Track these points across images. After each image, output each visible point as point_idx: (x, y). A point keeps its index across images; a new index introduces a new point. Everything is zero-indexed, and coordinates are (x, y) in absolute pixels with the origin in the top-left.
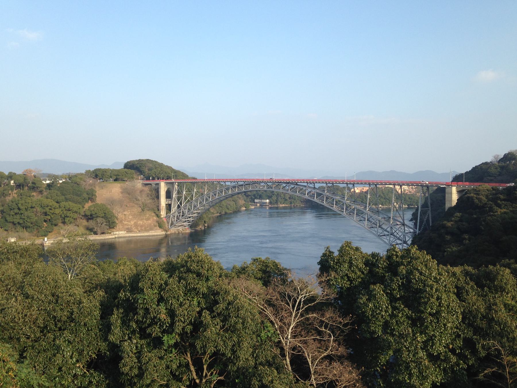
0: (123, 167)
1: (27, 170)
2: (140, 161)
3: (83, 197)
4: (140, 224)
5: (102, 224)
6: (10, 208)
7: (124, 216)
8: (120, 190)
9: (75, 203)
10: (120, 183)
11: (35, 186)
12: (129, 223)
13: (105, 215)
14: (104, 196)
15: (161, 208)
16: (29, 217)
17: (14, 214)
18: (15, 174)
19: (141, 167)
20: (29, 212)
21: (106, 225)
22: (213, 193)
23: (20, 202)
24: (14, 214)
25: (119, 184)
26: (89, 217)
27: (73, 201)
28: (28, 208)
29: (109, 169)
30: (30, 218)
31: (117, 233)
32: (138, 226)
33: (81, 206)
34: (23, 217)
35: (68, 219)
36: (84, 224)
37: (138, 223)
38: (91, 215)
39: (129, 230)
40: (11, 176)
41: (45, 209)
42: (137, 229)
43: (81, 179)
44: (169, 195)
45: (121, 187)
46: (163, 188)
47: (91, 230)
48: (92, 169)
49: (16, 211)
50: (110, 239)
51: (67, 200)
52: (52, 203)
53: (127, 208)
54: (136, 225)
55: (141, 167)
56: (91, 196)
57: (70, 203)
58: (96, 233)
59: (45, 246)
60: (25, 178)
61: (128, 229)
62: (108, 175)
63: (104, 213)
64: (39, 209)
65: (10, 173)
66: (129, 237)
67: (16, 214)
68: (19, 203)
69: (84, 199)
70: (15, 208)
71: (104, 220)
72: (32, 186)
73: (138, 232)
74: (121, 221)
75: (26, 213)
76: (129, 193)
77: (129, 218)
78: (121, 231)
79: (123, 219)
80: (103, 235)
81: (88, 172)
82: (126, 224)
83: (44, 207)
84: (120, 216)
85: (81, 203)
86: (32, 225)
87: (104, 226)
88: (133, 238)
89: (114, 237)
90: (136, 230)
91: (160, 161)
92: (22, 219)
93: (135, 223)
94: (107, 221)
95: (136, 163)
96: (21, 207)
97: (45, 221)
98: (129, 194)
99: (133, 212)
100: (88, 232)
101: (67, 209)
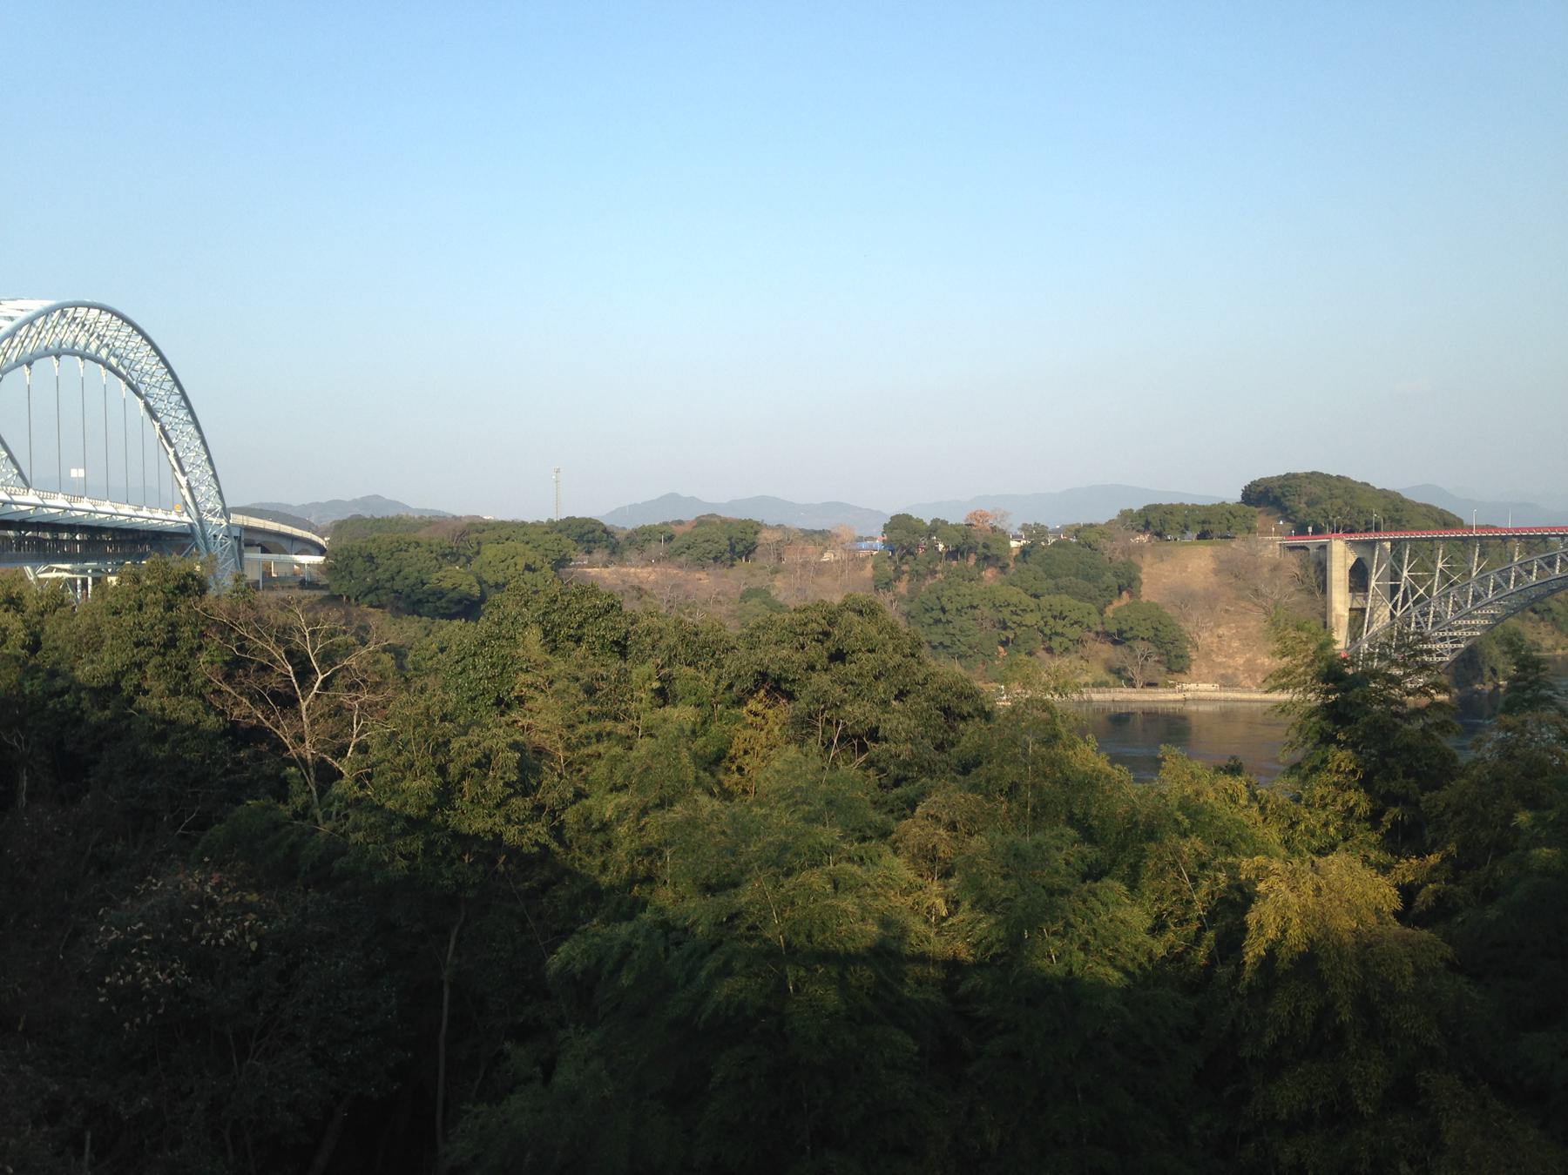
0: (1239, 499)
1: (975, 514)
2: (1286, 480)
3: (1103, 583)
4: (1263, 664)
5: (1146, 659)
6: (924, 607)
7: (1216, 640)
8: (1213, 566)
9: (1079, 601)
10: (1212, 545)
11: (989, 554)
12: (1231, 661)
13: (1156, 635)
14: (1164, 580)
15: (1334, 620)
16: (964, 631)
17: (931, 621)
18: (945, 523)
19: (1286, 496)
20: (965, 617)
21: (1158, 661)
22: (1498, 573)
23: (946, 593)
24: (931, 621)
25: (1209, 548)
26: (1118, 638)
27: (1074, 595)
28: (962, 608)
29: (1182, 504)
30: (967, 633)
31: (1193, 686)
32: (1257, 672)
33: (1093, 609)
34: (952, 631)
35: (1059, 639)
36: (1104, 655)
37: (1259, 661)
38: (1120, 632)
39: (1227, 682)
40: (938, 527)
41: (1001, 611)
42: (1253, 679)
43: (1102, 534)
44: (1359, 577)
45: (1215, 557)
46: (1341, 556)
47: (1120, 675)
48: (1137, 507)
49: (937, 614)
50: (1170, 701)
51: (1058, 589)
52: (1017, 596)
53: (1226, 615)
54: (1251, 668)
55: (1286, 496)
56: (1128, 582)
57: (1065, 597)
58: (1131, 683)
59: (249, 559)
60: (966, 533)
61: (1223, 676)
62: (1178, 523)
63: (1153, 628)
64: (987, 611)
65: (935, 521)
66: (1226, 700)
67: (938, 621)
68: (942, 596)
69: (1105, 590)
70: (935, 608)
71: (1153, 649)
72: (983, 553)
73: (1255, 688)
74: (1208, 654)
75: (958, 622)
76: (1236, 574)
77: (1230, 646)
78: (1205, 682)
79: (1215, 649)
80: (1148, 690)
81: (1126, 515)
82: (1220, 663)
83: (1001, 606)
84: (1205, 638)
85: (1095, 599)
86: (971, 652)
87: (1154, 669)
88: (1239, 704)
89: (1180, 696)
90: (1249, 682)
91: (1333, 471)
92: (950, 634)
93: (1248, 660)
94: (1161, 651)
95: (1276, 484)
96: (948, 606)
97: (1004, 644)
98: (1236, 576)
99: (1245, 628)
100: (1110, 678)
101: (1055, 613)
